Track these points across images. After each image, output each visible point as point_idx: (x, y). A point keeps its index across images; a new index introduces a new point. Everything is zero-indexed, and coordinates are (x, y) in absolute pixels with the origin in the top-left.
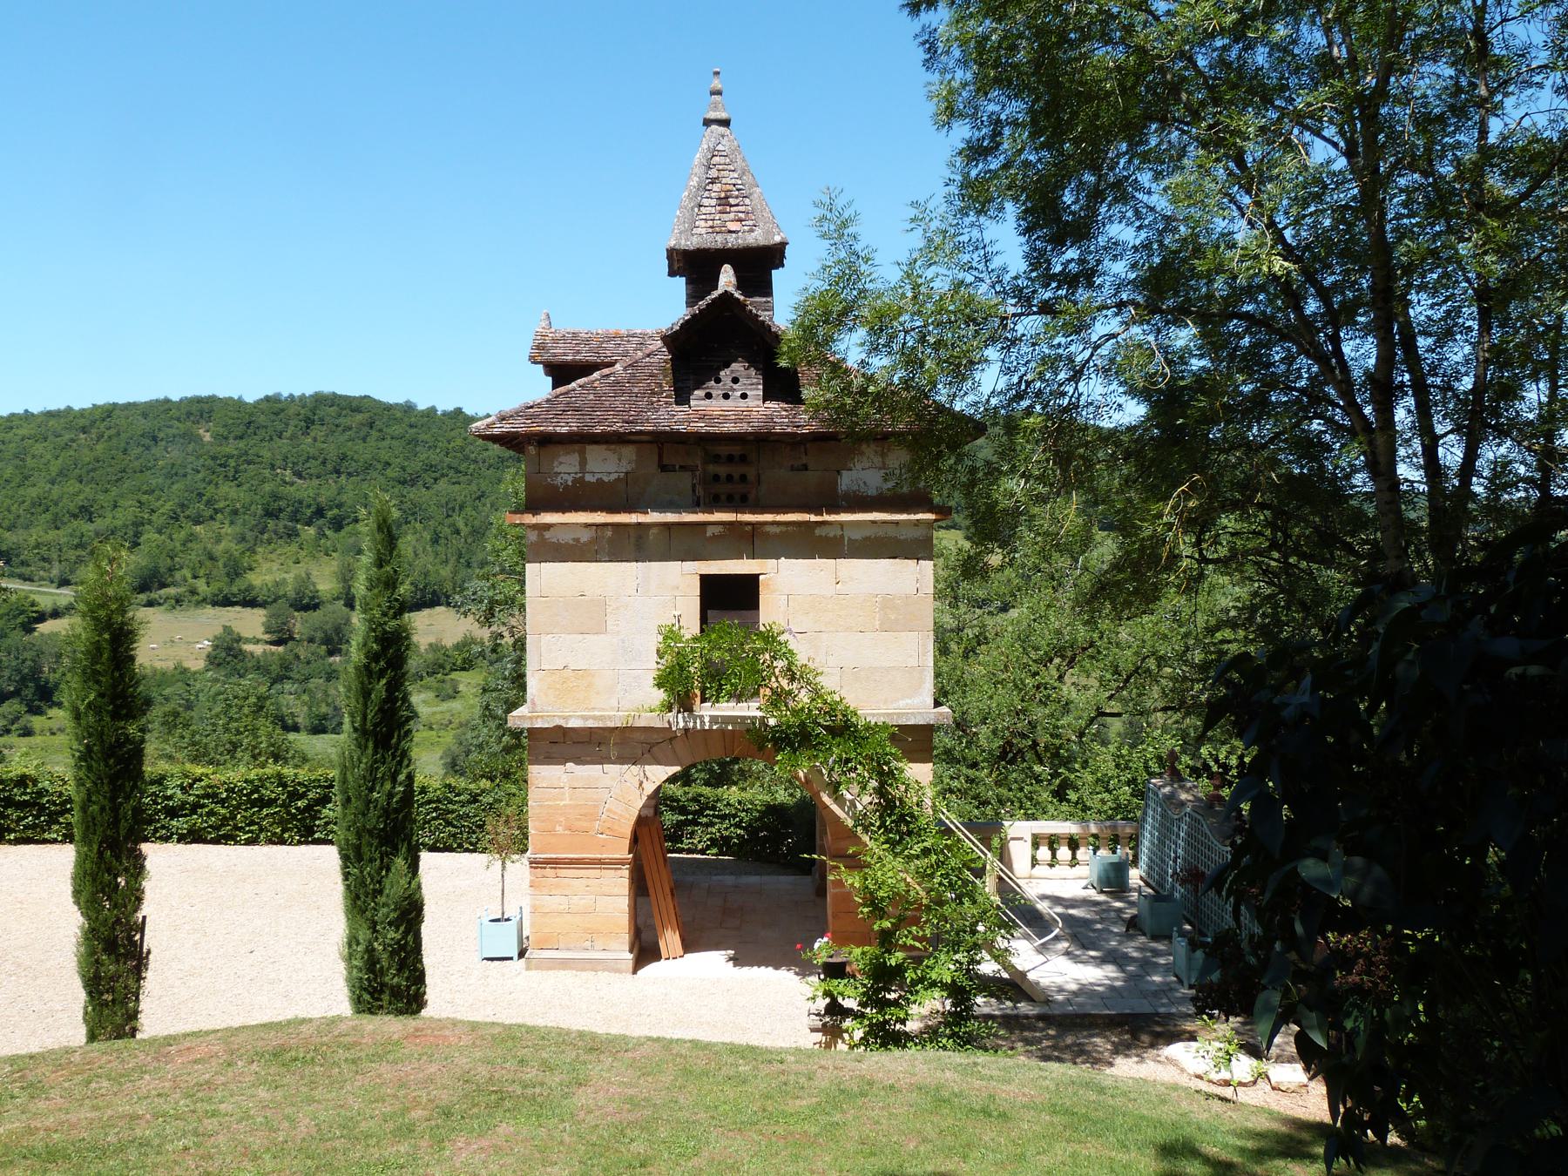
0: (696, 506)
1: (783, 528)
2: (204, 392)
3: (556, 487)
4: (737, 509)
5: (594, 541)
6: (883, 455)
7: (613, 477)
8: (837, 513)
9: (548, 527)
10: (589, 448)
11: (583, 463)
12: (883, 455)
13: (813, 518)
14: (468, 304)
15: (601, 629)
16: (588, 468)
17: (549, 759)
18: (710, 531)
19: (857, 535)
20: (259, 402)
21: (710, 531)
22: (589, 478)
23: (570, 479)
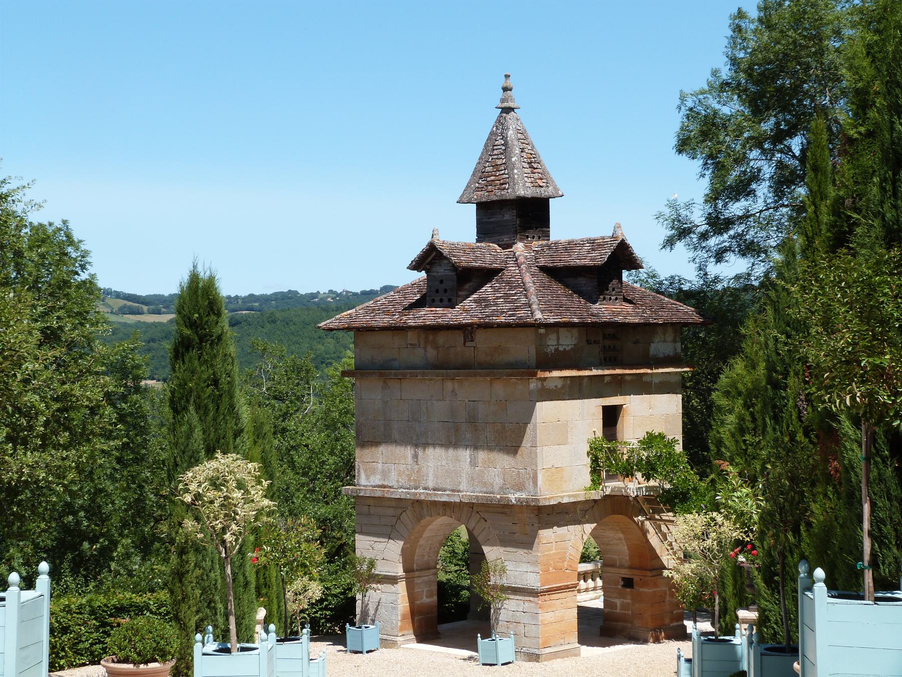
0: (597, 367)
1: (635, 377)
2: (284, 287)
3: (547, 354)
4: (579, 369)
5: (563, 387)
6: (664, 334)
7: (570, 347)
8: (632, 369)
9: (545, 379)
10: (561, 330)
11: (558, 339)
12: (664, 334)
13: (649, 371)
14: (335, 221)
15: (564, 442)
16: (561, 342)
17: (549, 525)
18: (645, 379)
19: (656, 380)
20: (306, 295)
21: (607, 379)
22: (561, 349)
23: (553, 348)
